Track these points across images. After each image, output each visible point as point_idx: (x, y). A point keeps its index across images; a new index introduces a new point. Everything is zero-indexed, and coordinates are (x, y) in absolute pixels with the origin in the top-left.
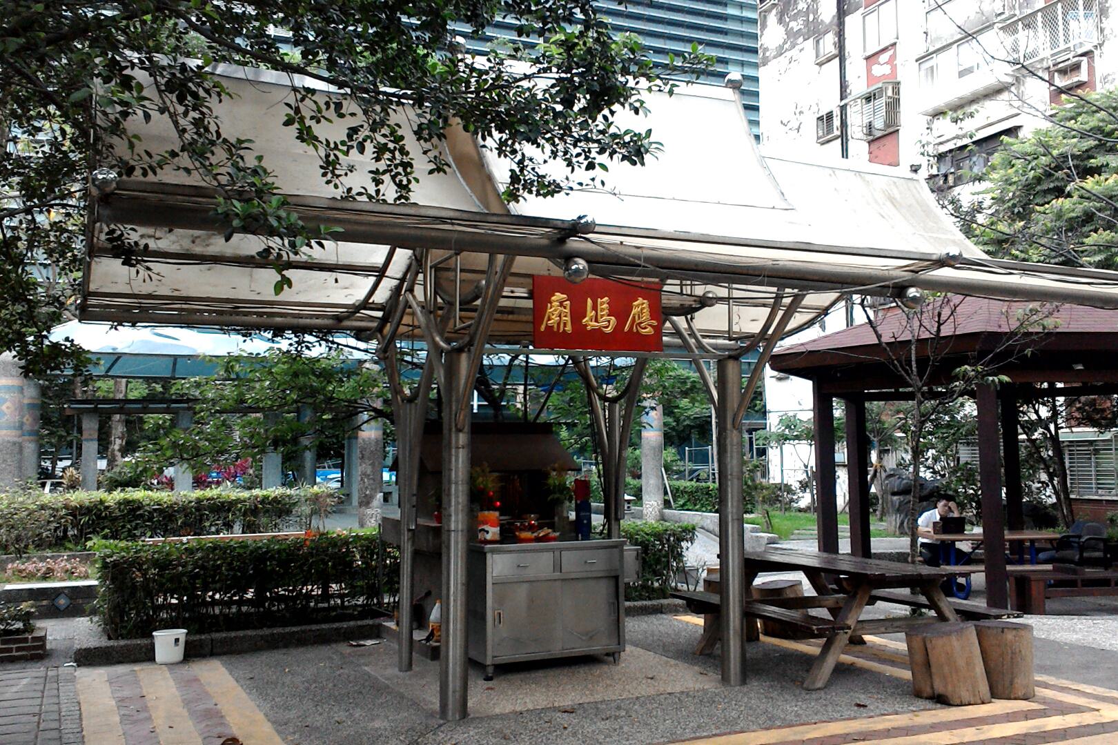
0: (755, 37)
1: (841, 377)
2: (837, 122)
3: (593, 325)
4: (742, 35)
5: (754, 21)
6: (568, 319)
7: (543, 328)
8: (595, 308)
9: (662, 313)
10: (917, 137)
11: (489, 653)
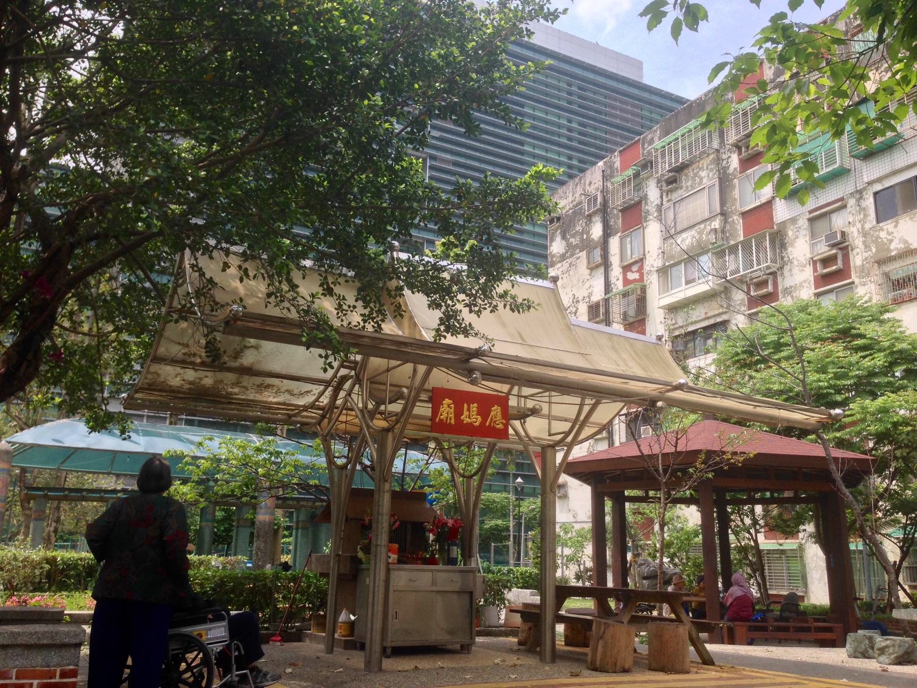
0: (545, 247)
1: (610, 480)
2: (602, 310)
3: (467, 420)
4: (534, 244)
5: (545, 237)
6: (452, 416)
7: (437, 420)
8: (469, 410)
9: (507, 416)
10: (657, 324)
11: (389, 640)
